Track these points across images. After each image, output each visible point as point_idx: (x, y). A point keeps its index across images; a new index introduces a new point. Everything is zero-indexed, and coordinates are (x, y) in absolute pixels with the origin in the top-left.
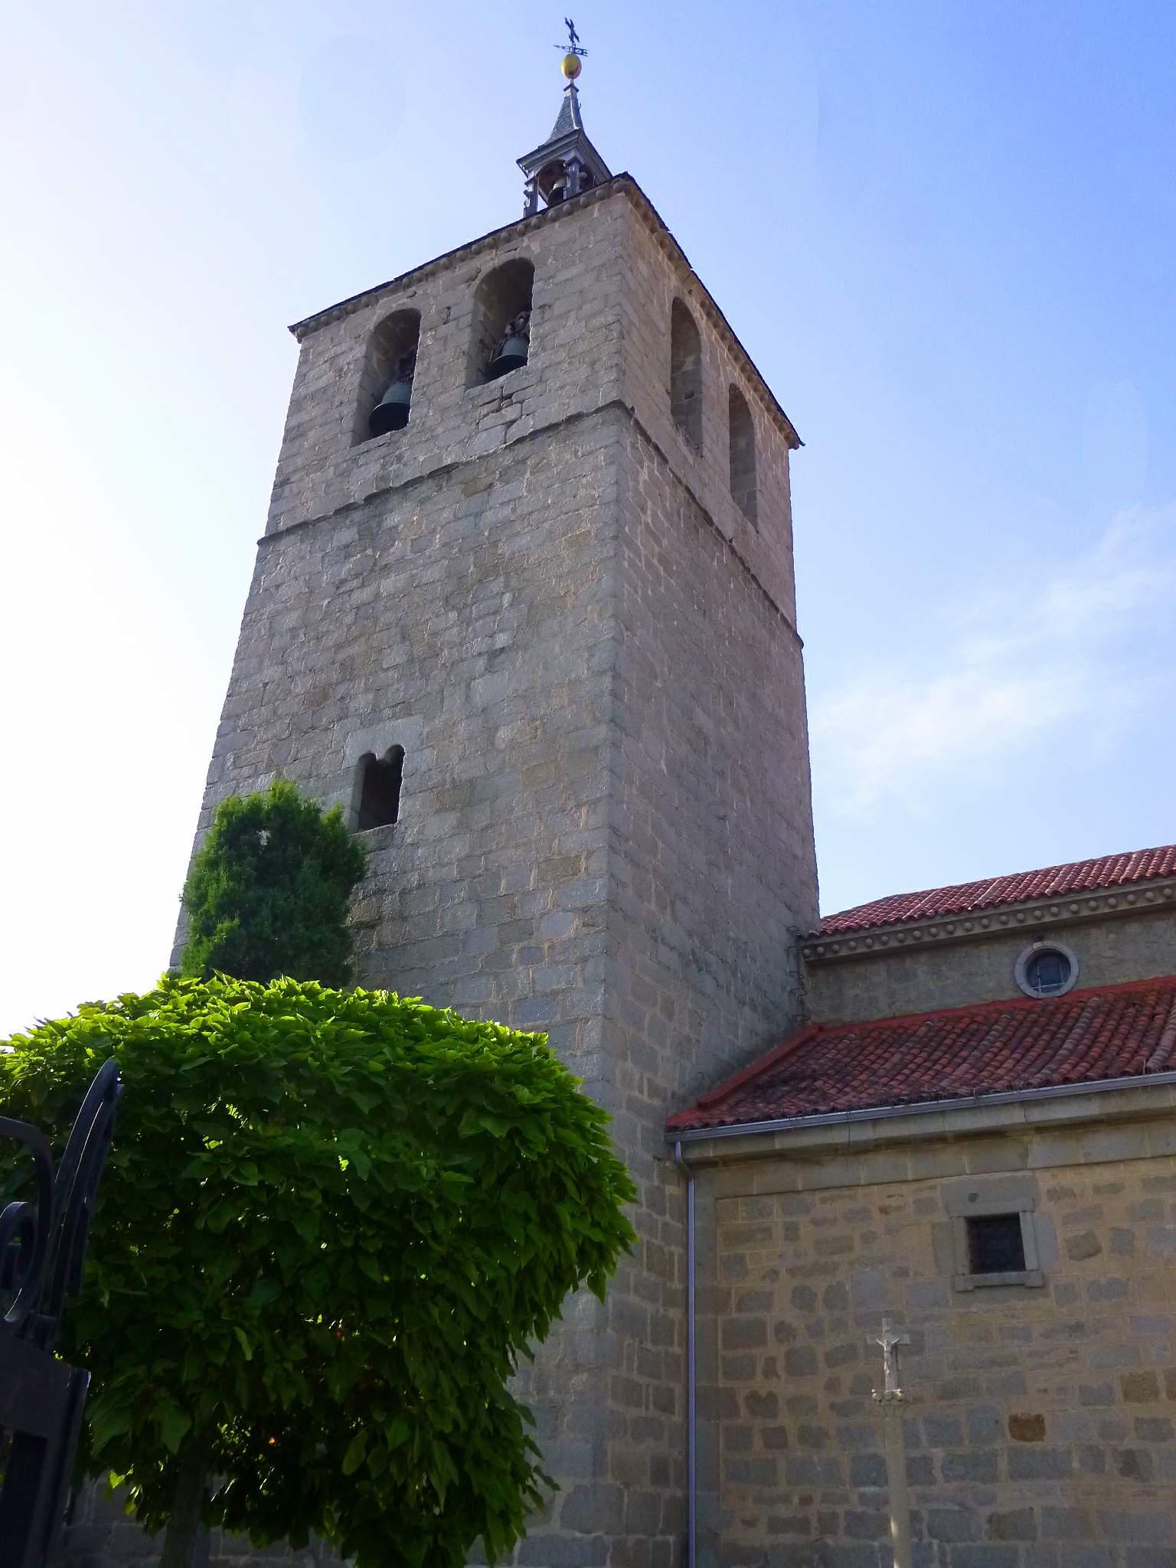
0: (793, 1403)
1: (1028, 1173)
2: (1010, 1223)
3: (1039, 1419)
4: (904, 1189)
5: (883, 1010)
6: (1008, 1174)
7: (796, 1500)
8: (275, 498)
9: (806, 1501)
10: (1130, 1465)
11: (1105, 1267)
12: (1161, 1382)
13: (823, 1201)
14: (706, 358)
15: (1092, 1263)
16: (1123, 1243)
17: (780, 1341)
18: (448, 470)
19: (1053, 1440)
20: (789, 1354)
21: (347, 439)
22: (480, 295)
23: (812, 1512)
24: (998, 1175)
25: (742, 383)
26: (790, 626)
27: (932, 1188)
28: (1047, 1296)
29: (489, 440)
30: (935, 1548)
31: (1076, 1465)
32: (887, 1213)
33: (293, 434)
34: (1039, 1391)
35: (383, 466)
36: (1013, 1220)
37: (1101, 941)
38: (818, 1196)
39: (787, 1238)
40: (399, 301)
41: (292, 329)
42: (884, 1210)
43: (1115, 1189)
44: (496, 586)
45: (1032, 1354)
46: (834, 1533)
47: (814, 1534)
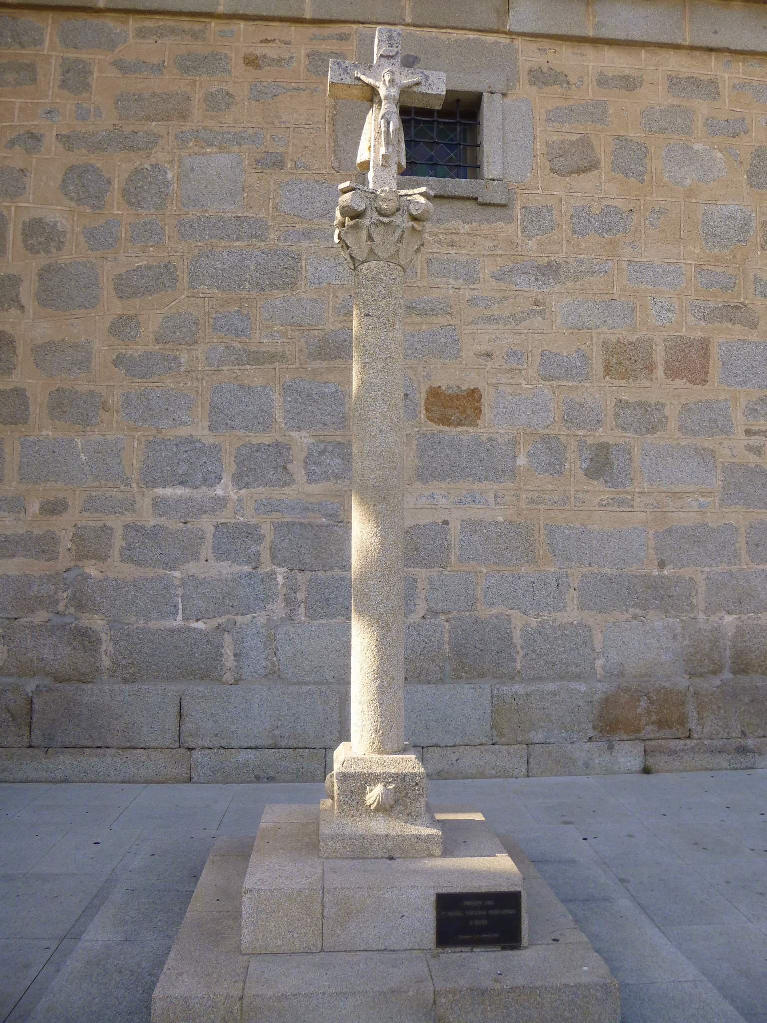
0: (43, 351)
1: (503, 40)
3: (474, 395)
4: (293, 31)
6: (472, 35)
7: (35, 507)
9: (53, 508)
10: (601, 463)
12: (660, 356)
13: (142, 34)
15: (585, 183)
17: (32, 250)
19: (492, 425)
20: (45, 273)
23: (63, 527)
24: (456, 35)
27: (342, 38)
28: (510, 220)
30: (280, 579)
31: (522, 461)
32: (258, 67)
34: (479, 355)
38: (133, 23)
39: (64, 84)
42: (252, 62)
43: (629, 83)
45: (473, 302)
46: (103, 558)
47: (64, 561)
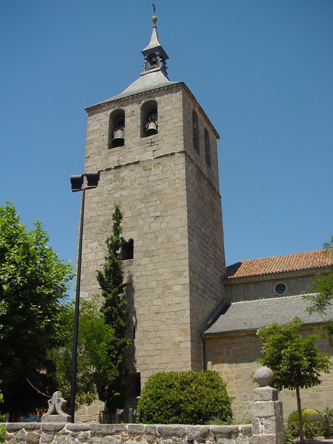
14: (199, 124)
18: (138, 162)
21: (107, 147)
25: (208, 129)
26: (218, 194)
29: (149, 155)
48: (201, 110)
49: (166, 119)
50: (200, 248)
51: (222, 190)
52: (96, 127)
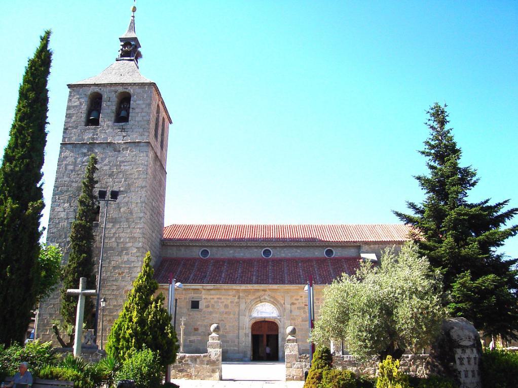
2: (198, 302)
5: (175, 256)
8: (64, 132)
11: (210, 309)
14: (160, 115)
16: (213, 306)
18: (110, 143)
19: (200, 331)
21: (83, 124)
22: (117, 97)
26: (165, 171)
29: (118, 140)
33: (68, 116)
35: (93, 135)
36: (198, 302)
37: (215, 249)
40: (97, 89)
41: (67, 85)
43: (213, 298)
44: (121, 176)
48: (163, 103)
49: (137, 110)
50: (150, 219)
51: (169, 168)
52: (76, 104)
